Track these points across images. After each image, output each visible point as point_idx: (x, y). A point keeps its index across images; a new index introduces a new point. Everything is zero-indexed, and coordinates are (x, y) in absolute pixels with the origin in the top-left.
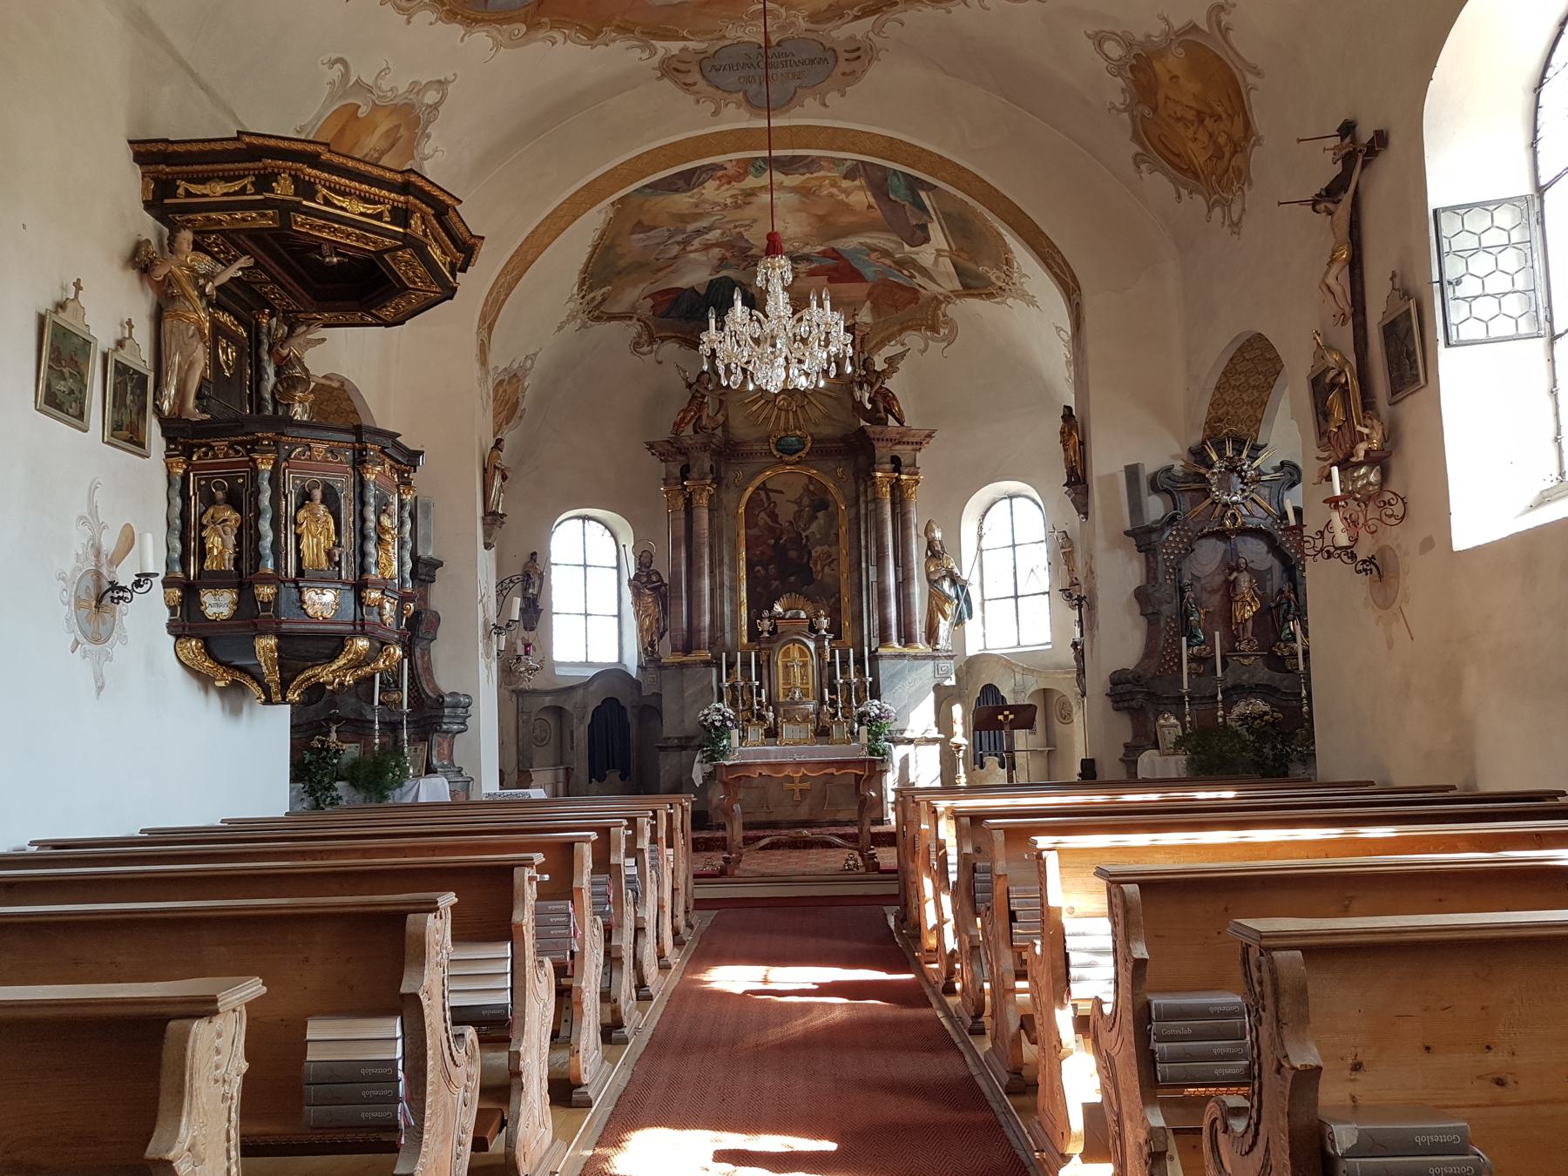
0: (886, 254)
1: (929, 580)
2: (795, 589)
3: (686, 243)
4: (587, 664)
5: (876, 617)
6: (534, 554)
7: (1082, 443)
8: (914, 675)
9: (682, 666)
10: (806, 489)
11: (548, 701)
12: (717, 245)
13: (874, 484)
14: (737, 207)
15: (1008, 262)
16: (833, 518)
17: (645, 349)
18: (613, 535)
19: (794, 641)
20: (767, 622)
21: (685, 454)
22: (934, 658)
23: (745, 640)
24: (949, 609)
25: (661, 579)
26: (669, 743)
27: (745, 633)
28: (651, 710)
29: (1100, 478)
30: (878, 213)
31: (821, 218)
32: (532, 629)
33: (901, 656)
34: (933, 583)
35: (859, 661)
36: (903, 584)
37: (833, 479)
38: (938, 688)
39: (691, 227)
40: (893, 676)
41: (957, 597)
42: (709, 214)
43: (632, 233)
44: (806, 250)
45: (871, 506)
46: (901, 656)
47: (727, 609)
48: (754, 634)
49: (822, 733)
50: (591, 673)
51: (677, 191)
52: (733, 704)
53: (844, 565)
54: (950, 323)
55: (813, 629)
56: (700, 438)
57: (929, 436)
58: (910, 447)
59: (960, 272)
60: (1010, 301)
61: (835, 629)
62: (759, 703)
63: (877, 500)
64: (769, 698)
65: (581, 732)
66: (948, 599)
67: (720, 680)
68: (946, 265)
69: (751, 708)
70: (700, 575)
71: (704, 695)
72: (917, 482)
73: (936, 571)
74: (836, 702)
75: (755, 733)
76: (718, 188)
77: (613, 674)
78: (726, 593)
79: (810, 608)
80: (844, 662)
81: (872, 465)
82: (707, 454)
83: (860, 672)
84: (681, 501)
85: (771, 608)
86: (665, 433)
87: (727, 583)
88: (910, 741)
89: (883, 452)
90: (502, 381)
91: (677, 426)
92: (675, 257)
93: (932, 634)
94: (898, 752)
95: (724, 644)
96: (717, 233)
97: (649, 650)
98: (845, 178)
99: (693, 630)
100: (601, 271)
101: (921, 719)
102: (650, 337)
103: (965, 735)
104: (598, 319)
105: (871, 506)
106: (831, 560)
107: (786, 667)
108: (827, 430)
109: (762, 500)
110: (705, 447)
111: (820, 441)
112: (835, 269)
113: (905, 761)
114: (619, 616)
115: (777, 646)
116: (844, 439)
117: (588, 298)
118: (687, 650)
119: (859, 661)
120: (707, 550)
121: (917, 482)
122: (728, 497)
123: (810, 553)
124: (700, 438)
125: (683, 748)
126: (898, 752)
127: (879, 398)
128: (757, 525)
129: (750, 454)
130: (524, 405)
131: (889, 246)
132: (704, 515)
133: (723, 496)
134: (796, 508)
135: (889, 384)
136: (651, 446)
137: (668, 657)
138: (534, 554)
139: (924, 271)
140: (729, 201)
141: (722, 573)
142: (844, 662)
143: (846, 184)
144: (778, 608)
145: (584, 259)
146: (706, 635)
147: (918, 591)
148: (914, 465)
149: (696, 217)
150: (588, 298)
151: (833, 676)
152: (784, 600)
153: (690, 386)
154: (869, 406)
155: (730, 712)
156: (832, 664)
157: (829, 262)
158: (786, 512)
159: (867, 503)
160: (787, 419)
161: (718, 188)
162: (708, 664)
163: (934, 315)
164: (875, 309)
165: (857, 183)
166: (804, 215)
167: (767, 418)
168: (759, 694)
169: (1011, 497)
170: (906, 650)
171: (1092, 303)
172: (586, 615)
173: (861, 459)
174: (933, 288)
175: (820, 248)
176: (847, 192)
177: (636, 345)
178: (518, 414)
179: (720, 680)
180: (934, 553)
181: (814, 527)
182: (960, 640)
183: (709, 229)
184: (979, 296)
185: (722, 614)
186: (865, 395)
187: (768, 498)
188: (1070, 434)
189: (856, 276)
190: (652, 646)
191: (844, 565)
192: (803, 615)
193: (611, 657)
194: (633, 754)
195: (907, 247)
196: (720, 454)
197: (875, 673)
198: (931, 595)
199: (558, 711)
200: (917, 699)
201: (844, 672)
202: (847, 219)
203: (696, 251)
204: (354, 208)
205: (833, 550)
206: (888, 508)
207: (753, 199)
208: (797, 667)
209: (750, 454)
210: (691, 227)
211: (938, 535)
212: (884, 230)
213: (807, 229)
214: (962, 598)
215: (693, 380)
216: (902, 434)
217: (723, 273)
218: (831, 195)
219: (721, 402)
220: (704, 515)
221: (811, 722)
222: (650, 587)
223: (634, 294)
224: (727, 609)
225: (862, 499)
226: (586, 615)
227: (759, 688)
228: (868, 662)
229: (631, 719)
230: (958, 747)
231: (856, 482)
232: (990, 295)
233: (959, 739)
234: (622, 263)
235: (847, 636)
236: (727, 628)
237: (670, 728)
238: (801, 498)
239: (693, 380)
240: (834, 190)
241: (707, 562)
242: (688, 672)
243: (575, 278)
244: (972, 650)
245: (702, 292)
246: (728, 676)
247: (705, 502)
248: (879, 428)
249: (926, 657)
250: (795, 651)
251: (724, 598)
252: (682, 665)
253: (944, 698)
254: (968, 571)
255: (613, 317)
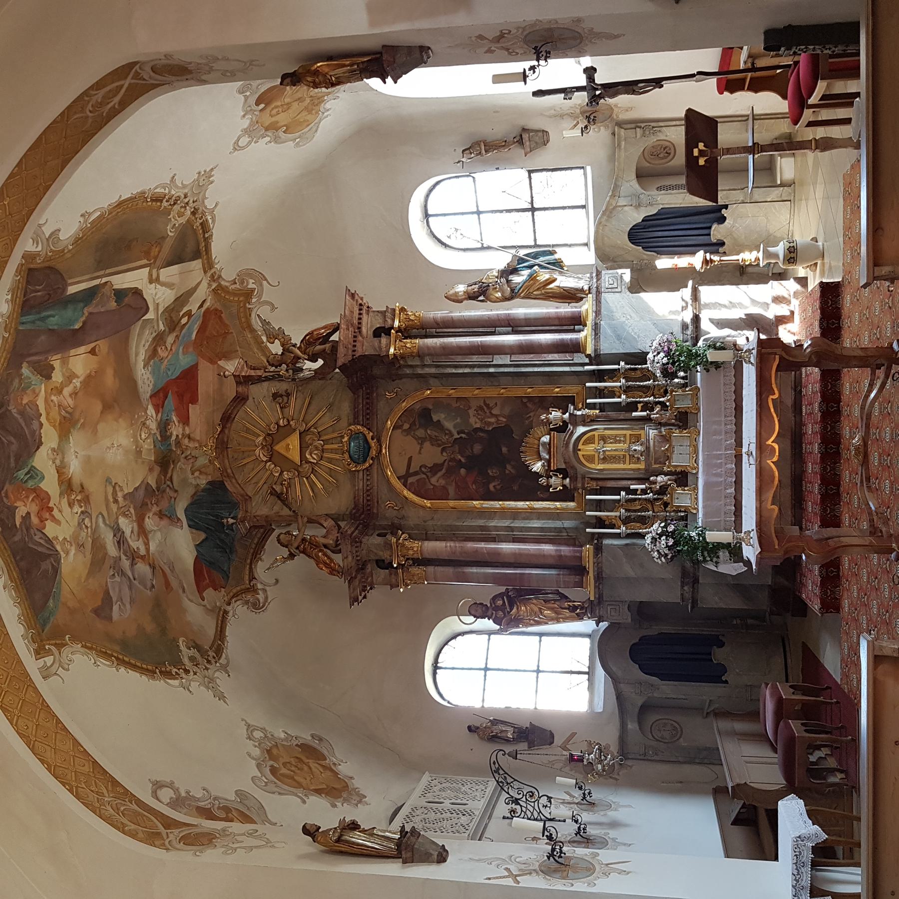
0: (159, 339)
1: (511, 298)
2: (516, 448)
3: (134, 556)
4: (590, 673)
5: (550, 357)
6: (470, 728)
7: (330, 58)
8: (618, 315)
9: (599, 578)
10: (408, 432)
11: (632, 726)
12: (140, 521)
13: (403, 357)
14: (86, 500)
15: (158, 199)
16: (438, 403)
17: (261, 597)
18: (454, 637)
19: (576, 449)
20: (553, 480)
21: (364, 564)
22: (598, 293)
23: (572, 504)
24: (544, 276)
25: (501, 595)
26: (688, 596)
27: (564, 504)
28: (643, 611)
29: (372, 24)
30: (103, 346)
31: (107, 407)
32: (552, 735)
33: (596, 328)
34: (513, 294)
35: (600, 376)
36: (514, 325)
37: (397, 403)
38: (636, 287)
39: (112, 550)
40: (619, 337)
41: (531, 267)
42: (95, 531)
43: (110, 619)
44: (153, 425)
45: (428, 361)
46: (596, 328)
47: (536, 524)
48: (565, 495)
49: (684, 420)
50: (600, 672)
51: (56, 570)
52: (645, 521)
53: (491, 392)
54: (243, 276)
55: (562, 428)
56: (346, 547)
57: (353, 296)
58: (365, 317)
59: (177, 258)
60: (210, 204)
61: (562, 403)
62: (644, 492)
63: (421, 354)
64: (641, 480)
65: (667, 690)
66: (532, 278)
67: (617, 536)
68: (169, 273)
69: (651, 502)
70: (497, 553)
71: (634, 554)
72: (402, 310)
73: (502, 290)
74: (646, 403)
75: (682, 498)
76: (58, 522)
77: (604, 649)
78: (518, 524)
79: (538, 431)
80: (600, 393)
81: (380, 359)
82: (364, 540)
83: (612, 375)
84: (415, 570)
85: (537, 475)
86: (340, 584)
87: (506, 523)
88: (696, 319)
89: (367, 347)
90: (273, 771)
91: (332, 571)
92: (153, 567)
93: (572, 296)
94: (711, 331)
95: (576, 529)
96: (122, 521)
97: (578, 612)
98: (48, 377)
99: (558, 564)
100: (155, 653)
101: (668, 307)
102: (247, 591)
103: (693, 253)
104: (219, 651)
105: (428, 361)
106: (485, 407)
107: (605, 460)
108: (346, 408)
109: (417, 480)
110: (356, 542)
111: (356, 416)
112: (180, 396)
113: (720, 324)
114: (541, 635)
115: (581, 470)
116: (354, 388)
117: (188, 664)
118: (579, 570)
119: (600, 376)
120: (470, 545)
121: (402, 310)
122: (413, 518)
123: (476, 430)
124: (346, 547)
125: (696, 581)
126: (711, 331)
127: (310, 350)
128: (444, 488)
129: (368, 491)
130: (306, 737)
131: (148, 336)
132: (433, 547)
133: (411, 523)
134: (427, 444)
135: (297, 340)
136: (355, 600)
137: (589, 592)
138: (470, 728)
139: (182, 300)
140: (77, 509)
141: (497, 528)
142: (600, 393)
143: (57, 377)
144: (537, 467)
145: (134, 675)
146: (565, 550)
147: (522, 309)
148: (383, 313)
149: (98, 545)
150: (188, 664)
151: (616, 407)
152: (528, 459)
153: (292, 556)
154: (320, 362)
155: (657, 527)
156: (602, 407)
157: (170, 402)
158: (431, 455)
159: (424, 366)
160: (332, 451)
161: (58, 522)
162: (598, 549)
163: (234, 293)
164: (227, 356)
165: (57, 364)
166: (101, 427)
167: (331, 472)
168: (635, 492)
169: (427, 216)
170: (590, 323)
171: (146, 43)
172: (538, 671)
173: (377, 371)
174: (203, 292)
175: (151, 411)
176: (70, 377)
177: (256, 606)
178: (315, 744)
179: (617, 536)
180: (481, 292)
181: (449, 425)
182: (579, 270)
183: (117, 531)
184: (207, 241)
185: (542, 529)
186: (310, 366)
187: (416, 473)
188: (316, 73)
189: (189, 376)
190: (575, 608)
191: (491, 392)
192: (546, 439)
193: (585, 644)
194: (694, 631)
195: (150, 315)
196: (366, 526)
197: (615, 358)
198: (527, 297)
199: (644, 709)
200: (646, 311)
201: (612, 393)
202: (110, 380)
203: (147, 544)
204: (557, 390)
205: (474, 404)
206: (430, 341)
207: (76, 481)
208: (604, 447)
209: (368, 491)
210: (112, 550)
211: (461, 288)
212: (126, 340)
213: (122, 423)
214: (532, 261)
215: (285, 552)
216: (349, 324)
217: (181, 514)
218: (74, 394)
219: (310, 521)
220: (433, 547)
221: (670, 433)
222: (511, 606)
223: (195, 613)
224: (536, 524)
225: (419, 371)
226: (538, 671)
227: (629, 491)
228: (602, 366)
229: (654, 630)
230: (706, 262)
231: (400, 377)
232: (205, 227)
233: (697, 260)
234: (150, 627)
235: (572, 390)
236: (558, 524)
237: (668, 592)
238: (417, 438)
239: (285, 552)
240: (67, 391)
241: (482, 545)
242: (607, 571)
243: (159, 685)
244: (589, 257)
245: (203, 536)
246: (613, 526)
247: (416, 545)
248: (341, 350)
249: (598, 301)
250: (587, 449)
251: (525, 527)
252: (599, 578)
253: (645, 280)
254: (502, 261)
255: (221, 633)
